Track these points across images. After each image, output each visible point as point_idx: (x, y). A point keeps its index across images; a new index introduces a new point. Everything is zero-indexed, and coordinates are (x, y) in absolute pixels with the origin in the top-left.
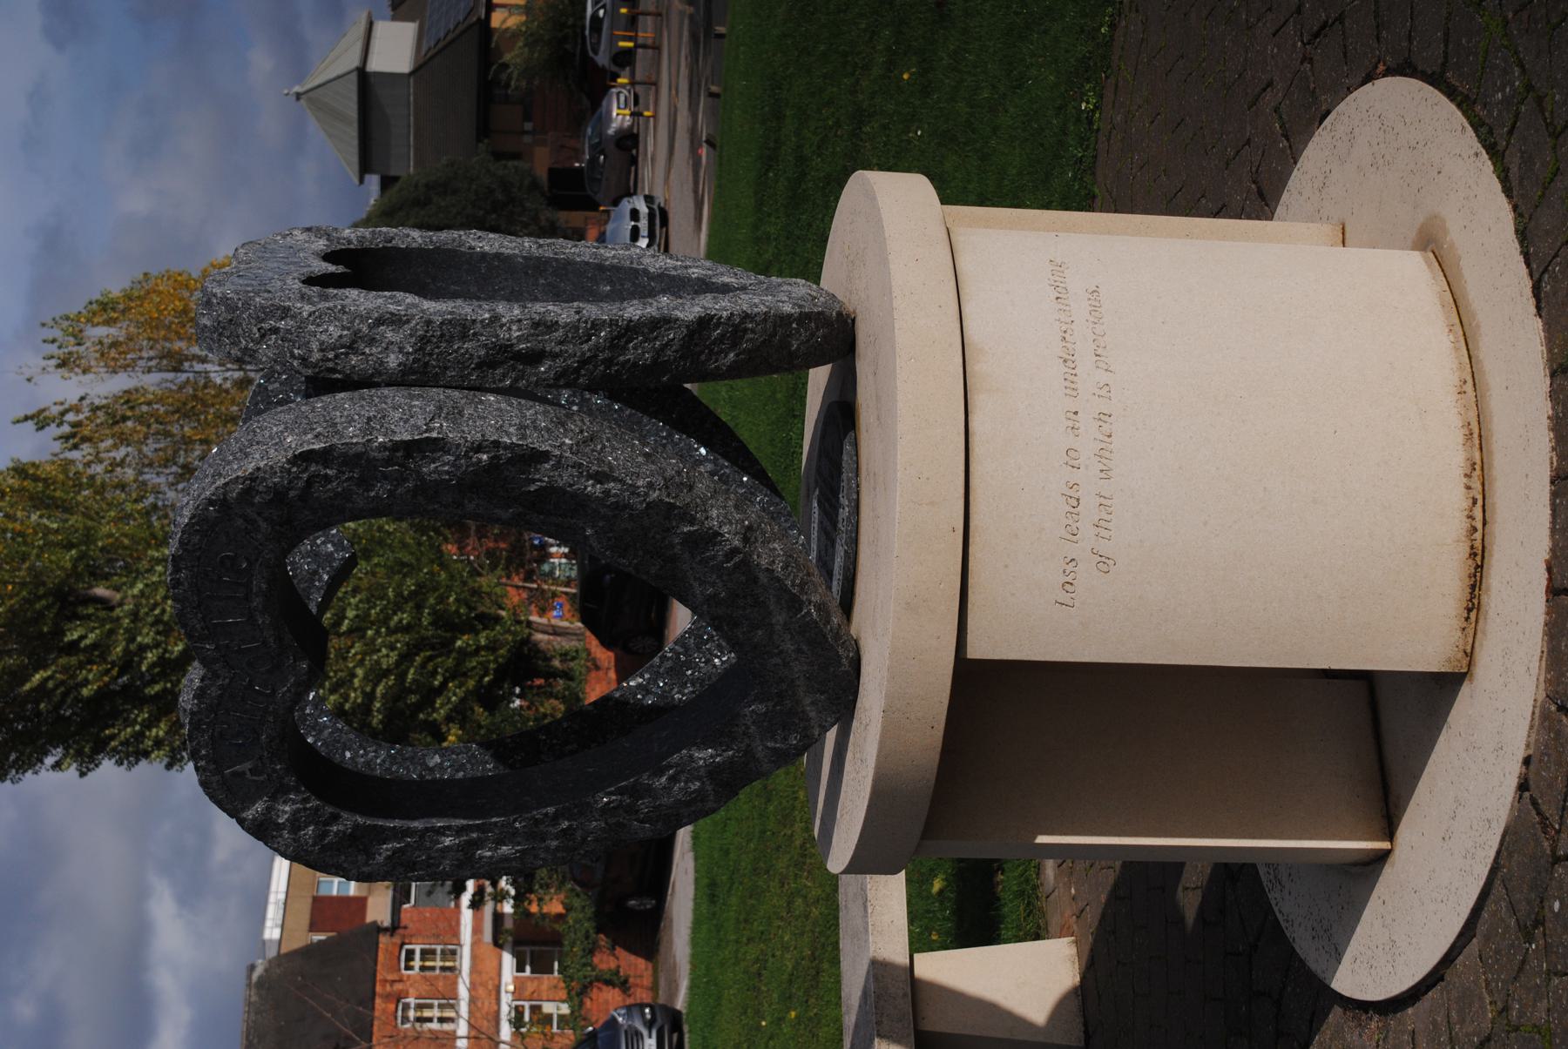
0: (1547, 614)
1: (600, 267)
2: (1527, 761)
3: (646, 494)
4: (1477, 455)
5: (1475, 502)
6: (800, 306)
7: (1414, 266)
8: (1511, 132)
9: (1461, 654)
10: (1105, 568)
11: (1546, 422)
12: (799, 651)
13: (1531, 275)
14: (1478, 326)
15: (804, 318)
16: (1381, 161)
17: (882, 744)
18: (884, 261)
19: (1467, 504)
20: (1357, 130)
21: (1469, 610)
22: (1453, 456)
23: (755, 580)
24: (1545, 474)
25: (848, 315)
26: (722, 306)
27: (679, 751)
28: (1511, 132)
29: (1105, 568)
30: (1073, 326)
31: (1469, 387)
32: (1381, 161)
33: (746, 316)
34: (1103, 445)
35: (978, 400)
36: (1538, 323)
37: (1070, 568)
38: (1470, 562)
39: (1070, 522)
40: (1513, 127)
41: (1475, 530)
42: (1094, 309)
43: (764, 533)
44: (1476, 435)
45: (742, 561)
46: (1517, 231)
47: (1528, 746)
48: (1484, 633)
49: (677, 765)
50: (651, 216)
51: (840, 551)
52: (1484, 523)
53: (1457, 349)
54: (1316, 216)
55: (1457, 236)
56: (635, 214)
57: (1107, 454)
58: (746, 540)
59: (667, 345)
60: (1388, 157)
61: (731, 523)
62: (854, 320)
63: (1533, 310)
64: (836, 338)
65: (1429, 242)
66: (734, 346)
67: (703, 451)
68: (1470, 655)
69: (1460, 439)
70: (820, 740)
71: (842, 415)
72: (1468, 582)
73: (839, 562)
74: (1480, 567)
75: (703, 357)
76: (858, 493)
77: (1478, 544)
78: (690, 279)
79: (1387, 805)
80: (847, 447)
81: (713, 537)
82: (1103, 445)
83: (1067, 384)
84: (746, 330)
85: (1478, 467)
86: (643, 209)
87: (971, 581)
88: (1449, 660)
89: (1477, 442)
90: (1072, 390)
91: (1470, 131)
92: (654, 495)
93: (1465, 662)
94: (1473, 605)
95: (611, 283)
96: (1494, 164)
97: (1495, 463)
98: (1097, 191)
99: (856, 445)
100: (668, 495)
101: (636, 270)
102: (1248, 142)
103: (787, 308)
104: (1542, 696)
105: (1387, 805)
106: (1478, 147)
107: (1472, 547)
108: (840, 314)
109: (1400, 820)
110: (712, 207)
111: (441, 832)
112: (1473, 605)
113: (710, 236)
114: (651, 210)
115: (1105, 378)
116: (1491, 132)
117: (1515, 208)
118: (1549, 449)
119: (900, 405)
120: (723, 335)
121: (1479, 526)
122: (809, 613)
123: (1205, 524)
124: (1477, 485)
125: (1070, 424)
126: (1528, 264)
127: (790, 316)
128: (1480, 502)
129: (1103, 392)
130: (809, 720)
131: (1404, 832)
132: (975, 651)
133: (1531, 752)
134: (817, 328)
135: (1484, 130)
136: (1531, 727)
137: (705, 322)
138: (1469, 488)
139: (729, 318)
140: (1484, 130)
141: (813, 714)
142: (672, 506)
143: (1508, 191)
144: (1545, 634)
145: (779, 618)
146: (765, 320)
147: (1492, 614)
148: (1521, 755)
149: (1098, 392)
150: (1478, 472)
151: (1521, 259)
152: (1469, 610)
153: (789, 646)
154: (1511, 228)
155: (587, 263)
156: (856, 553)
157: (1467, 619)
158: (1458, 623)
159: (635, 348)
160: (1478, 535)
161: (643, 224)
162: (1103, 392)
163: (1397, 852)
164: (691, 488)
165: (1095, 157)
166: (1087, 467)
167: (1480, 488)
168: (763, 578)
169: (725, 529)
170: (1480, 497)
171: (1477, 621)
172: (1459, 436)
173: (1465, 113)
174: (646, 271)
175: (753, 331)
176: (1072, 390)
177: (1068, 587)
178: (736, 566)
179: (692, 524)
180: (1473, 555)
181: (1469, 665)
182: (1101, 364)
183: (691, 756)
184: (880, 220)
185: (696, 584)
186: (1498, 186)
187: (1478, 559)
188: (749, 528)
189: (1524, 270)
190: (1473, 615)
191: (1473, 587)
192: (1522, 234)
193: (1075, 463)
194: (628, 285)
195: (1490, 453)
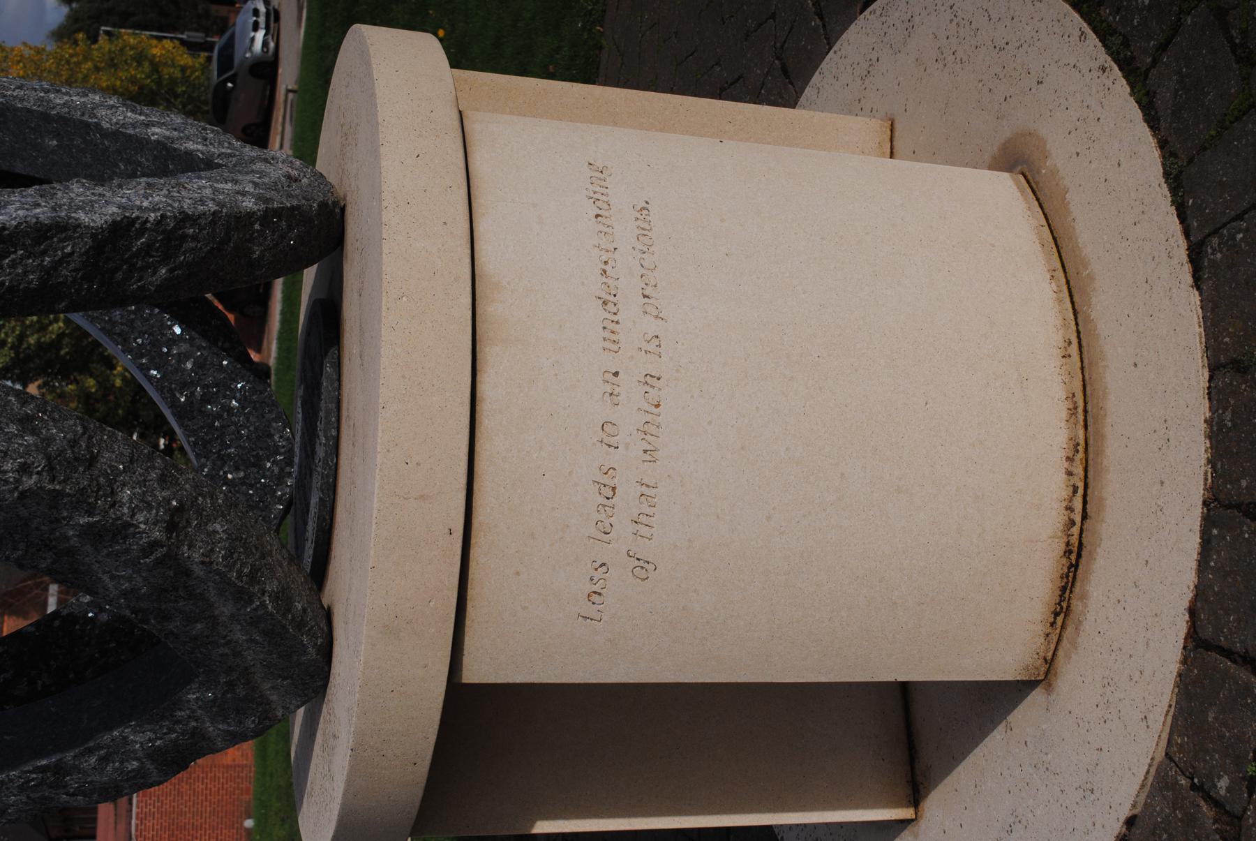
0: (1184, 662)
1: (45, 117)
2: (1130, 822)
3: (18, 481)
4: (1081, 433)
5: (1075, 491)
6: (267, 201)
7: (1005, 186)
8: (1163, 47)
9: (1041, 661)
10: (643, 574)
11: (1203, 426)
12: (251, 640)
13: (1187, 233)
14: (1091, 278)
15: (269, 217)
16: (950, 58)
17: (349, 783)
18: (376, 154)
19: (1066, 493)
20: (917, 19)
21: (1056, 614)
22: (1055, 435)
23: (188, 573)
24: (1197, 493)
25: (336, 203)
26: (144, 198)
27: (111, 729)
28: (1163, 47)
29: (643, 574)
30: (617, 255)
31: (1074, 350)
32: (950, 58)
33: (185, 219)
34: (649, 418)
35: (489, 353)
36: (1195, 297)
37: (597, 575)
38: (1064, 561)
39: (602, 517)
40: (1169, 41)
41: (1073, 523)
42: (643, 233)
43: (200, 511)
44: (1080, 410)
45: (166, 555)
46: (1166, 175)
47: (1134, 806)
48: (1074, 644)
49: (108, 747)
50: (268, 15)
51: (317, 482)
52: (1085, 516)
53: (1060, 301)
54: (855, 107)
55: (1061, 156)
56: (256, 12)
57: (652, 429)
58: (171, 527)
59: (60, 262)
60: (960, 54)
61: (149, 507)
62: (343, 209)
63: (1189, 280)
64: (321, 232)
65: (1018, 159)
66: (165, 259)
67: (177, 330)
68: (1050, 663)
69: (1064, 414)
70: (287, 721)
71: (328, 319)
72: (1060, 583)
73: (311, 526)
74: (1074, 567)
75: (119, 275)
76: (338, 429)
77: (1074, 540)
78: (148, 141)
79: (912, 769)
80: (328, 369)
81: (123, 530)
82: (649, 418)
83: (607, 334)
84: (184, 237)
85: (1081, 449)
86: (262, 9)
87: (476, 469)
88: (1027, 668)
89: (1081, 417)
90: (611, 339)
91: (1092, 38)
92: (30, 482)
93: (1043, 670)
94: (1063, 608)
95: (57, 136)
96: (1132, 86)
97: (1108, 451)
98: (604, 43)
99: (338, 366)
100: (53, 480)
101: (88, 125)
102: (773, 16)
103: (249, 204)
104: (1160, 755)
105: (912, 769)
106: (1104, 58)
107: (1068, 544)
108: (323, 205)
109: (928, 792)
110: (308, 12)
111: (150, 378)
112: (1063, 608)
113: (306, 32)
114: (268, 10)
115: (652, 326)
116: (1126, 44)
117: (1162, 144)
118: (1203, 461)
119: (384, 361)
120: (148, 248)
121: (1078, 519)
122: (263, 604)
123: (769, 518)
124: (1079, 471)
125: (608, 388)
126: (1182, 217)
127: (251, 214)
128: (1081, 491)
129: (652, 347)
130: (269, 703)
131: (934, 803)
132: (473, 673)
133: (1136, 811)
134: (290, 228)
135: (1116, 40)
136: (1143, 786)
137: (121, 229)
138: (1069, 473)
139: (158, 222)
140: (1116, 40)
141: (274, 698)
142: (59, 494)
143: (1152, 121)
144: (1177, 685)
145: (225, 609)
146: (213, 222)
147: (1087, 626)
148: (1125, 812)
149: (645, 346)
150: (1081, 455)
151: (1173, 210)
152: (1056, 614)
153: (240, 636)
154: (1158, 170)
155: (29, 111)
156: (334, 501)
157: (1052, 624)
158: (1041, 629)
159: (13, 265)
160: (1075, 530)
161: (262, 20)
162: (652, 347)
163: (923, 824)
164: (93, 460)
165: (605, 11)
166: (627, 446)
167: (1082, 473)
168: (198, 571)
169: (140, 517)
170: (1081, 485)
171: (1063, 627)
172: (1062, 411)
173: (1083, 16)
174: (98, 125)
175: (194, 238)
176: (611, 339)
177: (595, 598)
178: (158, 562)
179: (91, 515)
180: (1068, 552)
181: (1047, 673)
182: (650, 309)
183: (125, 738)
184: (373, 95)
185: (106, 578)
186: (1137, 114)
187: (1073, 557)
188: (180, 509)
189: (1175, 225)
190: (1060, 619)
191: (1063, 589)
192: (1176, 180)
193: (613, 441)
194: (78, 141)
195: (1101, 437)
